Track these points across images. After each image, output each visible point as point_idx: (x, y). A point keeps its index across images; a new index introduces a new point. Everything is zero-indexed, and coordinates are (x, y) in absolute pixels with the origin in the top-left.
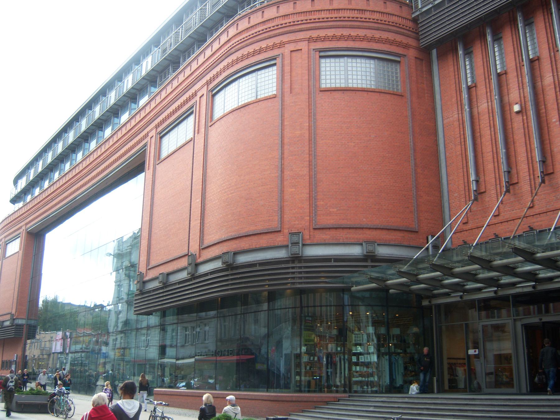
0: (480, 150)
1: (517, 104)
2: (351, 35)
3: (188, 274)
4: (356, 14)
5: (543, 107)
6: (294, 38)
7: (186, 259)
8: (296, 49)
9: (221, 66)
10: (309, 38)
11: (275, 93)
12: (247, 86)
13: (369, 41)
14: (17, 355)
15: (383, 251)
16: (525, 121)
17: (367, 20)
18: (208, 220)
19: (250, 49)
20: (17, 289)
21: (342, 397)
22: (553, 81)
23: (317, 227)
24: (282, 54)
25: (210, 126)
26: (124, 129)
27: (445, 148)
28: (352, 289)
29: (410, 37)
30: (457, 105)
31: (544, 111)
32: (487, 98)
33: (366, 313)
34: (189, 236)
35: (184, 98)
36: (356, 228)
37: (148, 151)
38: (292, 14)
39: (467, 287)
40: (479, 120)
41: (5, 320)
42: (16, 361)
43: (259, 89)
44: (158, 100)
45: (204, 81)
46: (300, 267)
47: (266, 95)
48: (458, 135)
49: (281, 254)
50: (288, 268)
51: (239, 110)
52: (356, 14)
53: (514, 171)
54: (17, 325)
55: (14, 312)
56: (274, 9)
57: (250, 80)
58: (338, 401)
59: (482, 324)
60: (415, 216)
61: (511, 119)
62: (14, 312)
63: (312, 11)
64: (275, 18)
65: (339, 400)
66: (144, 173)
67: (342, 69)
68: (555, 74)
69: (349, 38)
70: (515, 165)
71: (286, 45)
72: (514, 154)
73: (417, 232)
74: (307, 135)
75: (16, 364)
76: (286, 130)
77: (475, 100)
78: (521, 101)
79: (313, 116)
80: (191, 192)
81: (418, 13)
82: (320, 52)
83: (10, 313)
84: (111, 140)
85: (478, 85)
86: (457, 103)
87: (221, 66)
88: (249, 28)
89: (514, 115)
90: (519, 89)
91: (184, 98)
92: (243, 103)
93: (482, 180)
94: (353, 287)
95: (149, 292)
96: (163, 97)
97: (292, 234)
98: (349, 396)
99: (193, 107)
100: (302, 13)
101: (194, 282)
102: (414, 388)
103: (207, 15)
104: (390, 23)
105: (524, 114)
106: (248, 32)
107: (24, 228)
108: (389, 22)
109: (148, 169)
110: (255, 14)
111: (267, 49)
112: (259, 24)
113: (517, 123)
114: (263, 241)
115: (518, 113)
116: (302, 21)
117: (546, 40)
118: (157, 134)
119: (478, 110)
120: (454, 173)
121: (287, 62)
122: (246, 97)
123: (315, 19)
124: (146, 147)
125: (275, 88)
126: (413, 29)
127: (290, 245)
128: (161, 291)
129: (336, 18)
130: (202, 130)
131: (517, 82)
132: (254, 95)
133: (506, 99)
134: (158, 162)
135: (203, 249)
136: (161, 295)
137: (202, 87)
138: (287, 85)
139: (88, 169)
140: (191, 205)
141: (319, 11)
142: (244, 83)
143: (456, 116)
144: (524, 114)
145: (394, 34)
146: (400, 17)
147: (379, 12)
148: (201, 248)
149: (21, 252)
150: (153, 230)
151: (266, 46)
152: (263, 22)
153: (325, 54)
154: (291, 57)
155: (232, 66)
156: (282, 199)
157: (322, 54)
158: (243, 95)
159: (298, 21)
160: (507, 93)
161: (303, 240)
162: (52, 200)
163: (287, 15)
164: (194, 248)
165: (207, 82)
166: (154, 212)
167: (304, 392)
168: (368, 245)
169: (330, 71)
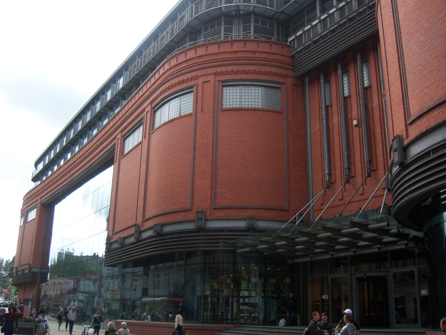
0: (333, 152)
1: (355, 119)
2: (245, 70)
3: (135, 239)
4: (249, 55)
5: (372, 122)
6: (205, 73)
7: (134, 228)
8: (206, 81)
9: (159, 91)
10: (215, 73)
11: (192, 112)
12: (174, 106)
13: (257, 74)
14: (33, 295)
15: (261, 225)
16: (361, 132)
17: (257, 59)
18: (148, 201)
19: (176, 80)
20: (33, 246)
21: (230, 327)
22: (378, 103)
23: (216, 207)
24: (197, 84)
25: (152, 134)
26: (105, 129)
27: (311, 150)
28: (237, 251)
29: (289, 70)
30: (320, 119)
31: (372, 125)
32: (338, 114)
33: (255, 268)
34: (137, 212)
35: (137, 112)
36: (243, 208)
37: (116, 149)
38: (205, 55)
39: (359, 244)
40: (333, 130)
41: (25, 269)
42: (32, 299)
43: (182, 109)
44: (127, 108)
45: (149, 101)
46: (203, 236)
47: (186, 113)
48: (319, 141)
49: (191, 226)
50: (195, 236)
51: (168, 124)
52: (249, 55)
53: (353, 168)
54: (34, 273)
55: (31, 263)
56: (193, 52)
57: (176, 102)
58: (227, 330)
59: (392, 271)
60: (286, 199)
61: (352, 130)
62: (31, 263)
63: (218, 53)
64: (194, 58)
65: (228, 329)
66: (113, 165)
67: (238, 94)
68: (380, 98)
69: (243, 72)
70: (353, 163)
71: (200, 78)
72: (353, 155)
73: (288, 211)
74: (211, 143)
75: (32, 301)
76: (197, 139)
77: (330, 115)
78: (358, 117)
79: (216, 129)
80: (139, 181)
81: (294, 52)
82: (223, 82)
83: (29, 264)
84: (97, 136)
85: (333, 105)
86: (320, 117)
87: (159, 91)
88: (177, 65)
89: (354, 127)
90: (358, 109)
91: (137, 112)
92: (171, 118)
93: (333, 173)
94: (238, 250)
95: (113, 250)
96: (126, 110)
97: (198, 212)
98: (235, 327)
99: (143, 119)
100: (211, 54)
101: (138, 244)
102: (282, 322)
103: (156, 52)
104: (274, 60)
105: (360, 127)
106: (176, 68)
107: (39, 201)
108: (273, 59)
109: (116, 162)
110: (181, 55)
111: (187, 80)
112: (183, 62)
113: (356, 132)
114: (180, 217)
115: (356, 126)
116: (211, 60)
117: (375, 74)
118: (122, 137)
119: (332, 123)
120: (316, 168)
121: (200, 90)
122: (174, 115)
123: (220, 59)
124: (115, 146)
125: (192, 109)
126: (291, 63)
127: (197, 220)
128: (120, 250)
129: (235, 58)
130: (147, 136)
131: (356, 104)
132: (178, 113)
133: (349, 115)
134: (121, 157)
135: (145, 221)
136: (120, 253)
137: (148, 105)
138: (199, 107)
139: (80, 159)
140: (139, 189)
141: (223, 53)
142: (172, 104)
143: (319, 127)
144: (360, 127)
145: (276, 68)
146: (281, 55)
147: (266, 52)
148: (143, 220)
149: (37, 219)
150: (117, 206)
151: (187, 78)
152: (185, 61)
153: (226, 84)
154: (203, 86)
155: (165, 92)
156: (193, 188)
157: (224, 84)
158: (172, 112)
159: (209, 61)
160: (350, 111)
161: (205, 216)
162: (58, 181)
163: (201, 56)
164: (139, 221)
165: (151, 102)
166: (118, 193)
167: (210, 323)
168: (249, 220)
169: (230, 96)
